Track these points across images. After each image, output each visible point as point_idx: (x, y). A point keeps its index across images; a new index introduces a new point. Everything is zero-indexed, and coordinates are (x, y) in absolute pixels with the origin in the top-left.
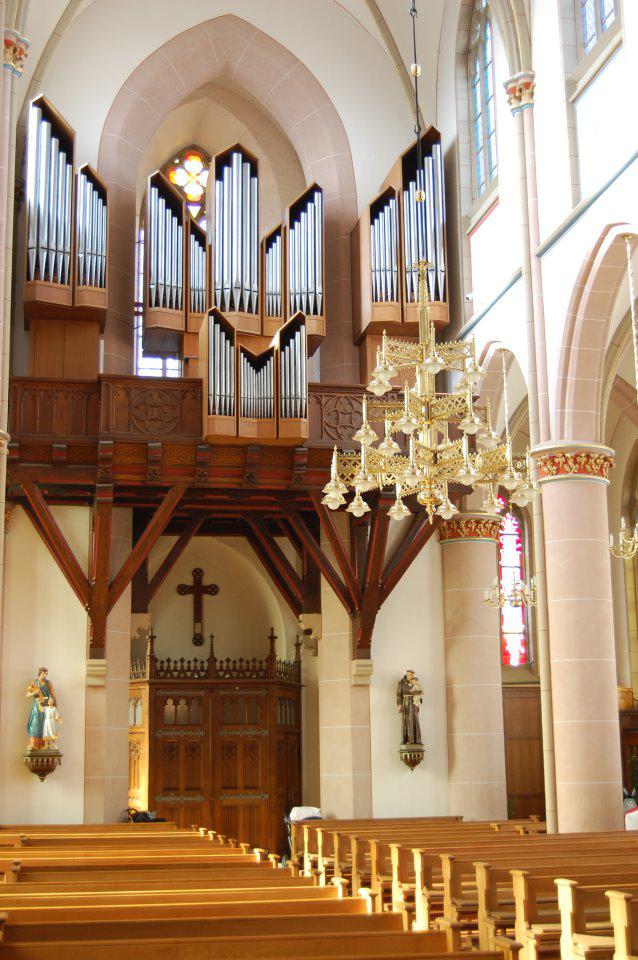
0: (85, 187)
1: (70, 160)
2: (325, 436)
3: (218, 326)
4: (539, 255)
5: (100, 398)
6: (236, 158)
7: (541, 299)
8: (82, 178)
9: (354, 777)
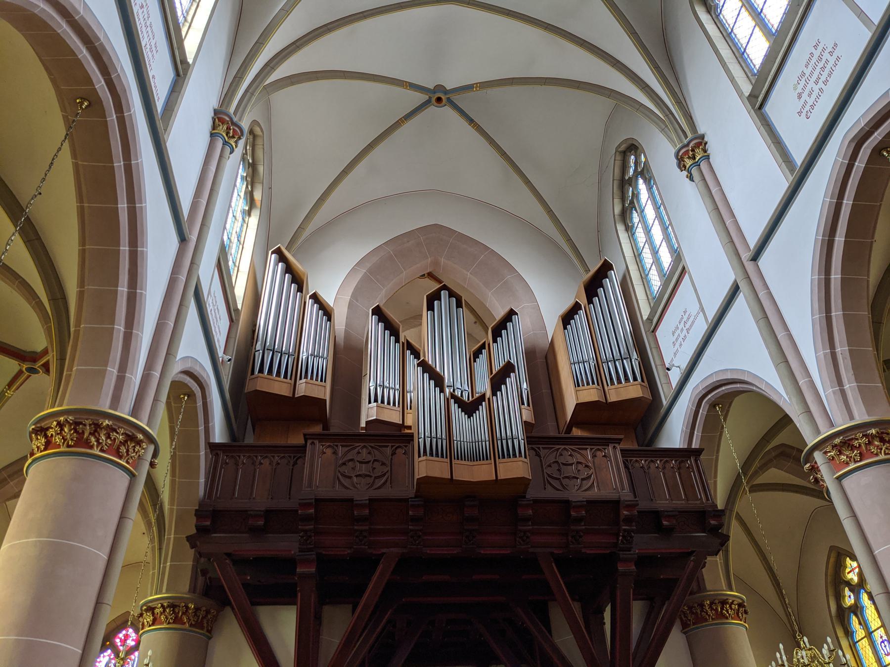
0: (311, 309)
1: (300, 289)
2: (547, 486)
3: (426, 375)
4: (755, 258)
5: (304, 464)
6: (444, 294)
7: (770, 294)
8: (309, 302)
9: (132, 330)
